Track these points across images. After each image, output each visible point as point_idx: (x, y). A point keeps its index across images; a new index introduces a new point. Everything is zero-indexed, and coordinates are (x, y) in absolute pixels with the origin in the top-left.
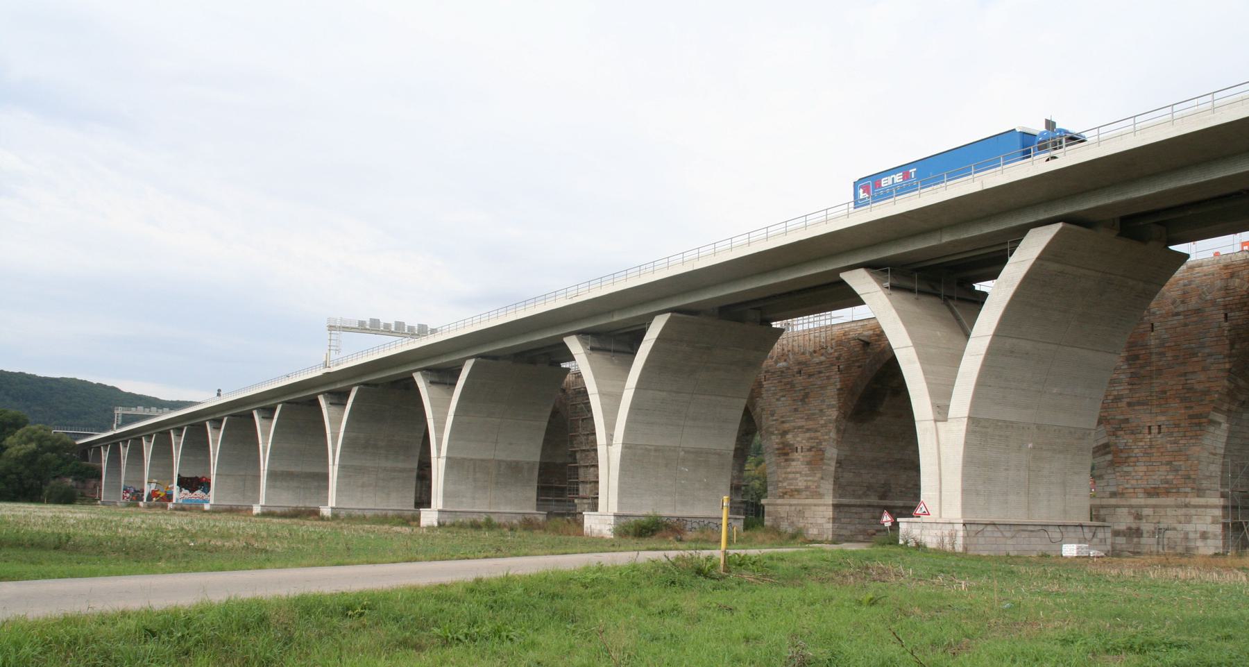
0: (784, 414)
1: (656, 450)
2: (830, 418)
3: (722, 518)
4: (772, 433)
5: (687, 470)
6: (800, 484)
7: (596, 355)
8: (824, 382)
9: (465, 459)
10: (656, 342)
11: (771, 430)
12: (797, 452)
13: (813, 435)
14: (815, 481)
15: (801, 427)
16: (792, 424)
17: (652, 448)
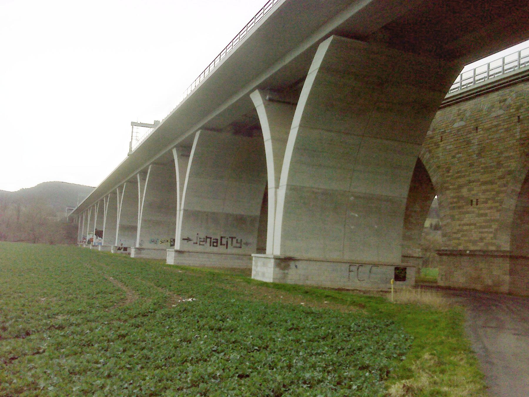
0: (460, 170)
1: (323, 194)
2: (509, 169)
3: (391, 289)
4: (447, 189)
5: (357, 215)
6: (474, 235)
7: (276, 106)
8: (502, 135)
9: (199, 212)
10: (318, 72)
11: (445, 185)
12: (472, 205)
13: (489, 187)
14: (491, 232)
15: (479, 180)
16: (467, 178)
17: (320, 191)
